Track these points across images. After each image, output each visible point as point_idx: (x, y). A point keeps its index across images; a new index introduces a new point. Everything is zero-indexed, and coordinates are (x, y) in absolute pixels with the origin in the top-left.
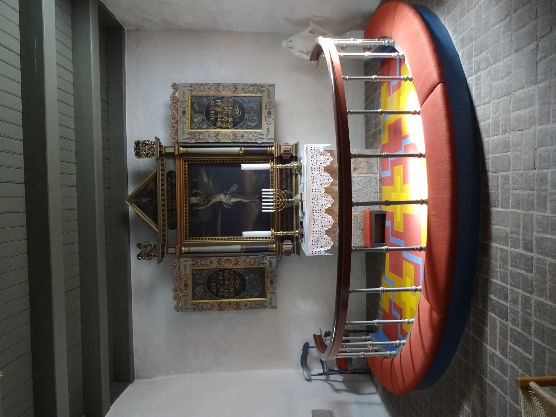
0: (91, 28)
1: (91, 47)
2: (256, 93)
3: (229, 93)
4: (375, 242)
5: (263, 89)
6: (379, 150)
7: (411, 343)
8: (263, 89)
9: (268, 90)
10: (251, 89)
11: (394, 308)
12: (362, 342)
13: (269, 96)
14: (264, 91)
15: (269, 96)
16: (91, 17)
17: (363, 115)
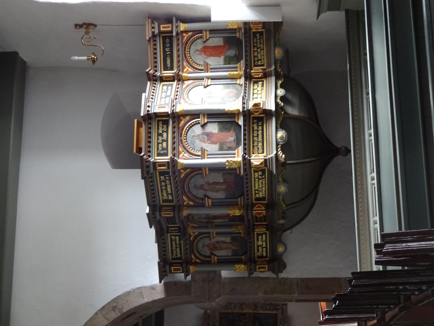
0: (12, 126)
1: (11, 143)
2: (272, 311)
3: (250, 311)
4: (204, 147)
5: (278, 307)
6: (280, 82)
7: (148, 25)
8: (278, 307)
9: (282, 309)
10: (268, 307)
11: (240, 126)
12: (404, 214)
13: (283, 313)
14: (279, 309)
15: (283, 313)
16: (13, 116)
17: (222, 38)
